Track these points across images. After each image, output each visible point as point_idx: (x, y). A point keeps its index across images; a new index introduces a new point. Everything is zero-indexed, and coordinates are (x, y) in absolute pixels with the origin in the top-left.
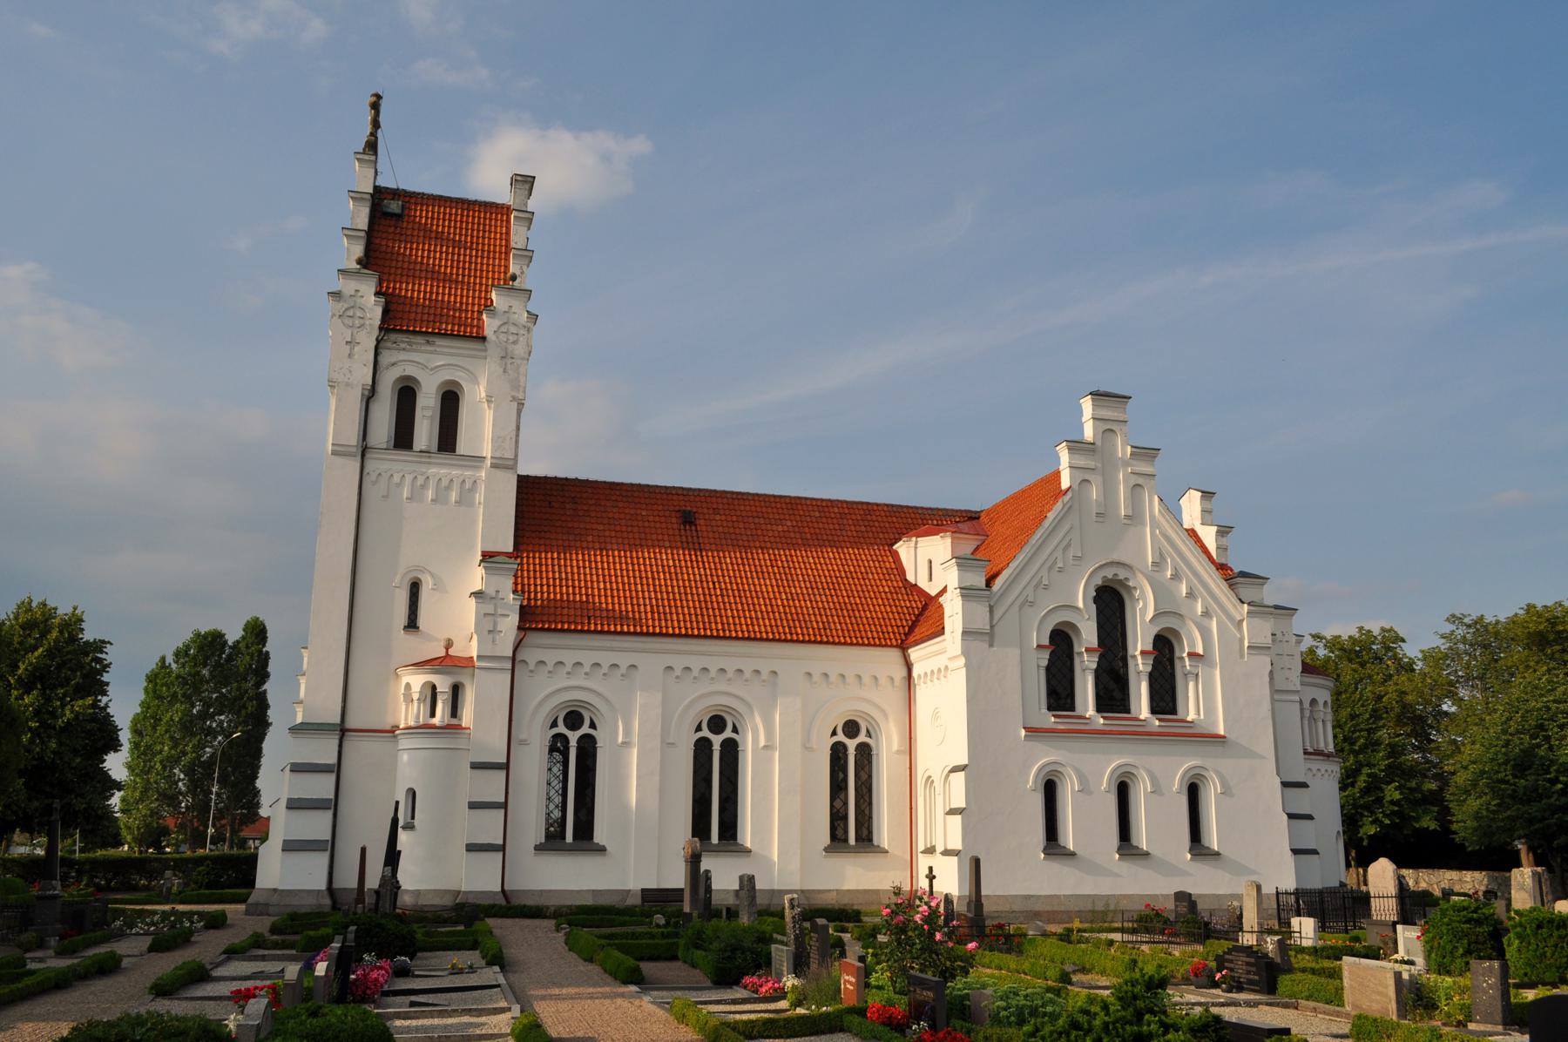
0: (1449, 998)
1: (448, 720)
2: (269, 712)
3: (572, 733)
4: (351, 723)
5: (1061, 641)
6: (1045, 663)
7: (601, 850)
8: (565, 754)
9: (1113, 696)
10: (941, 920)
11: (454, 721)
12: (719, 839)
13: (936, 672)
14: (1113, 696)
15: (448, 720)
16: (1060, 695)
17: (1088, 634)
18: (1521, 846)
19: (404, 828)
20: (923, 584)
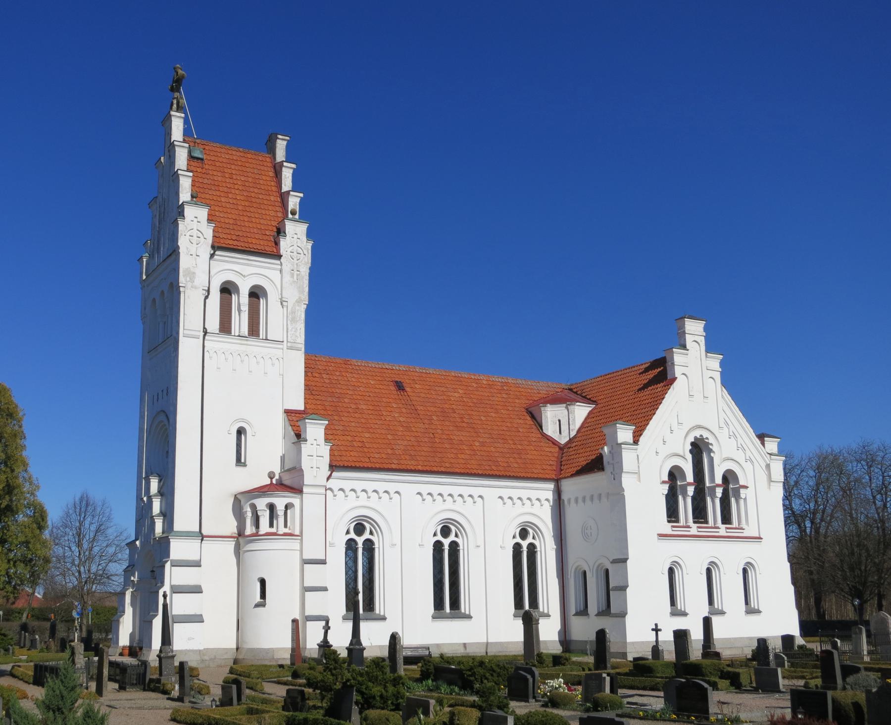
0: (393, 716)
1: (254, 531)
2: (236, 525)
3: (359, 538)
4: (204, 532)
5: (674, 475)
6: (666, 492)
7: (469, 617)
8: (355, 551)
9: (700, 514)
10: (6, 617)
11: (273, 530)
12: (450, 610)
13: (580, 500)
14: (700, 514)
15: (254, 531)
16: (672, 514)
17: (688, 468)
18: (836, 639)
19: (578, 614)
20: (555, 436)
